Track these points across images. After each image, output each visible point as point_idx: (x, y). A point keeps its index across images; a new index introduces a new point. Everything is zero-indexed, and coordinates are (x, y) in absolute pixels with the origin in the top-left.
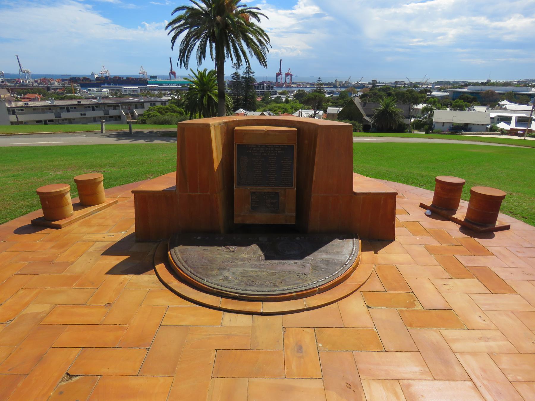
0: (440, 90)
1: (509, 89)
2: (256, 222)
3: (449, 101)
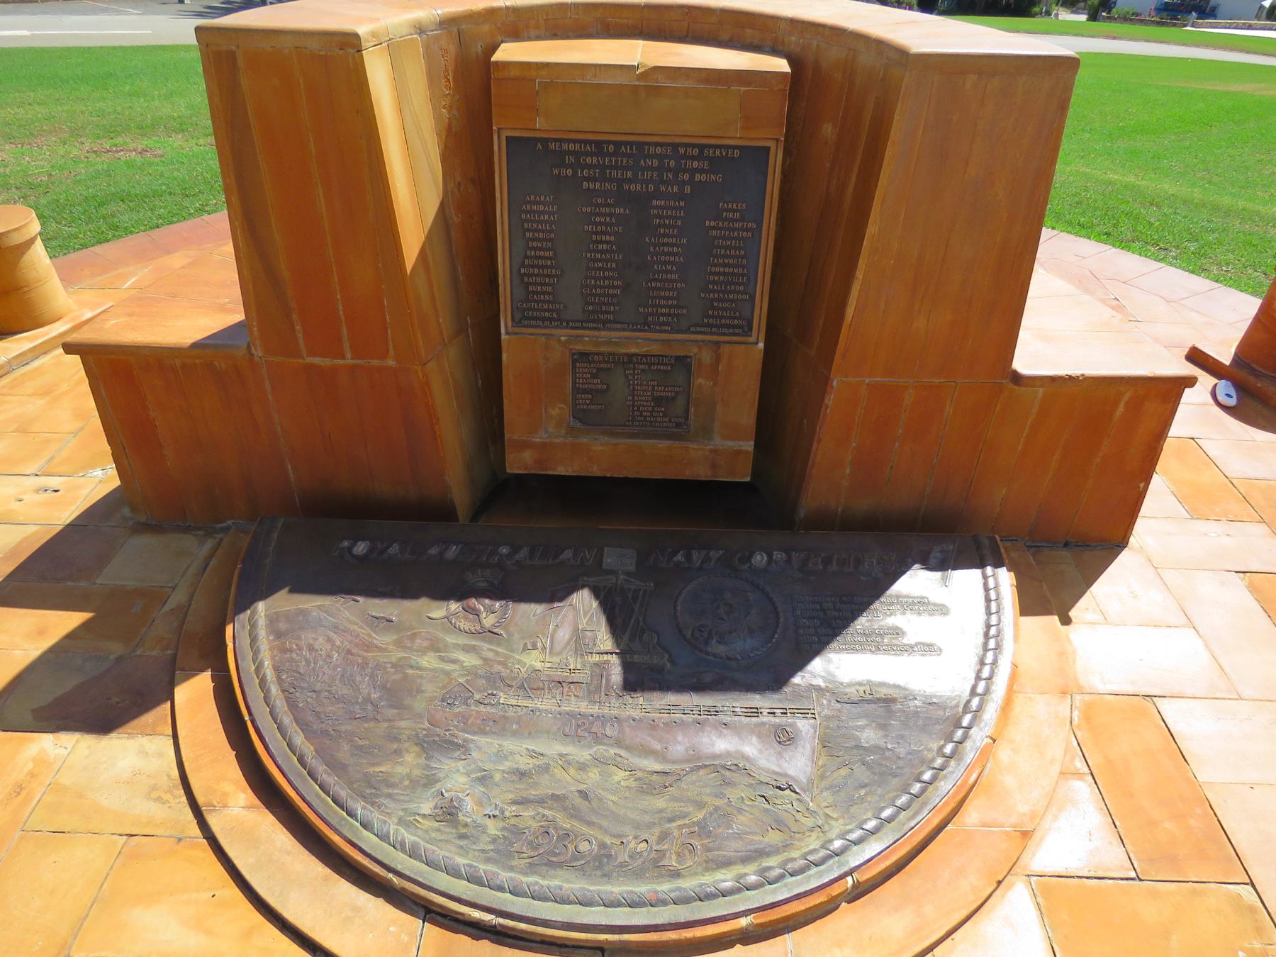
2: (596, 471)
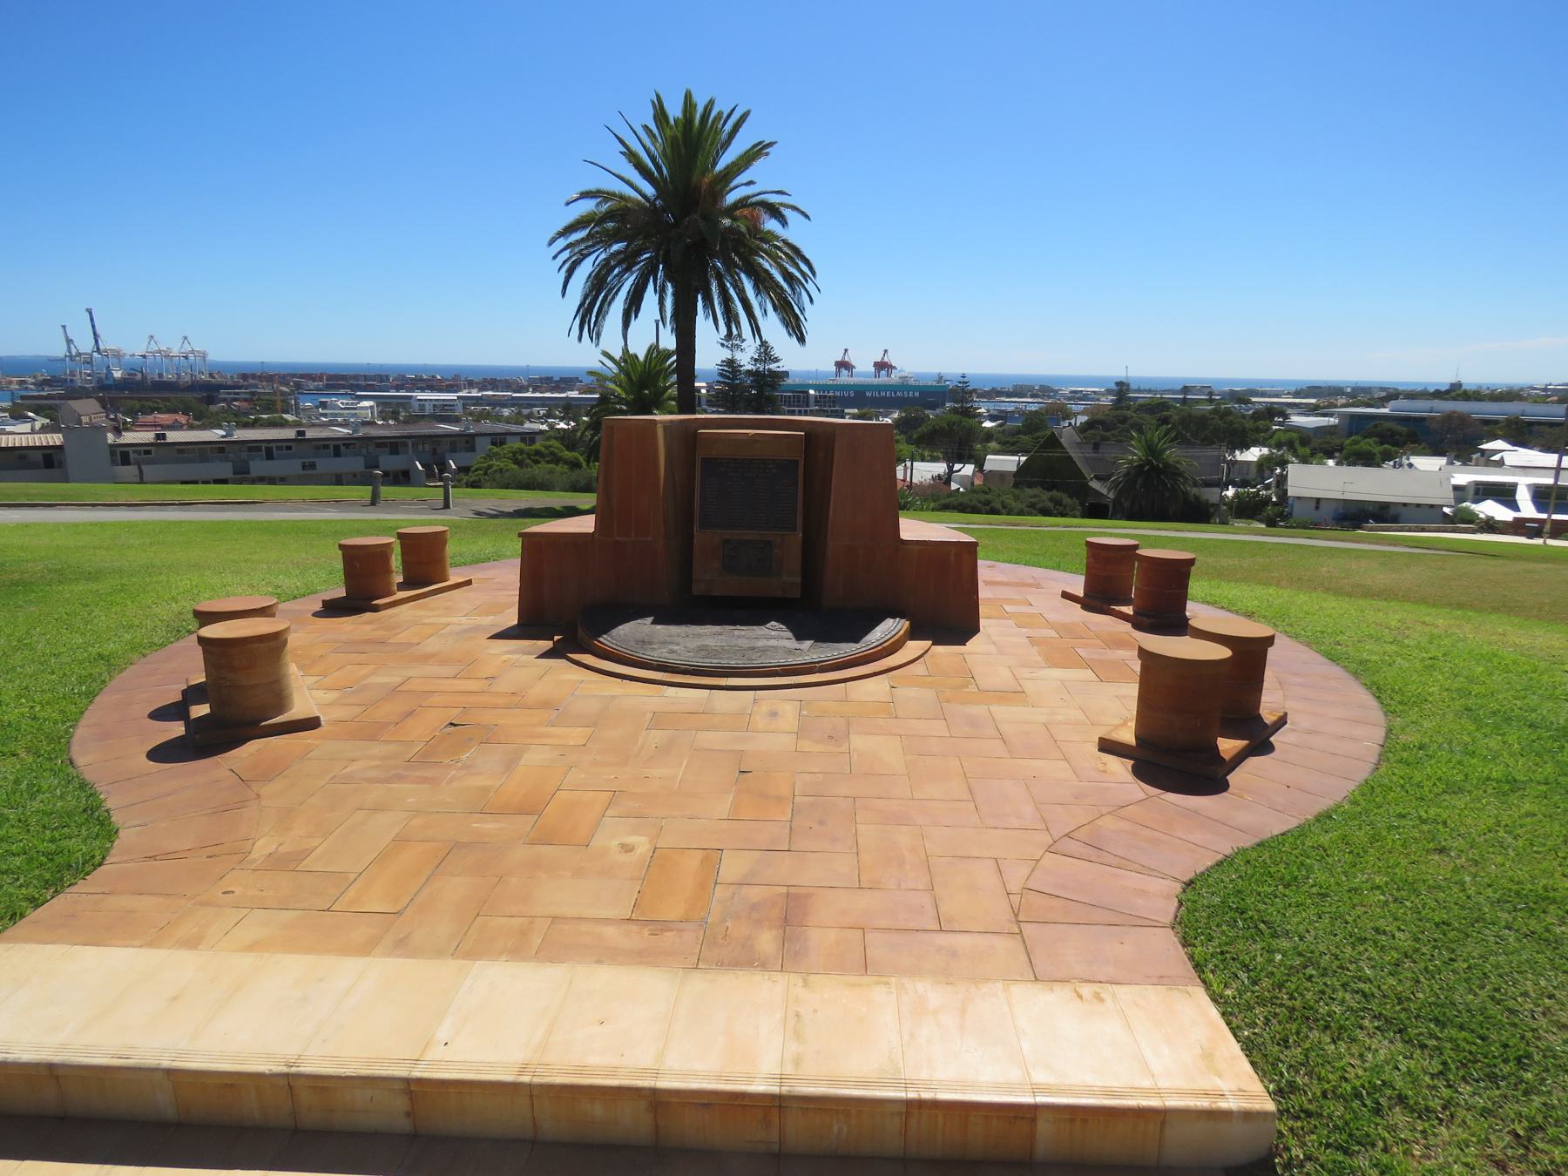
0: (1312, 410)
1: (1512, 408)
3: (1337, 441)
